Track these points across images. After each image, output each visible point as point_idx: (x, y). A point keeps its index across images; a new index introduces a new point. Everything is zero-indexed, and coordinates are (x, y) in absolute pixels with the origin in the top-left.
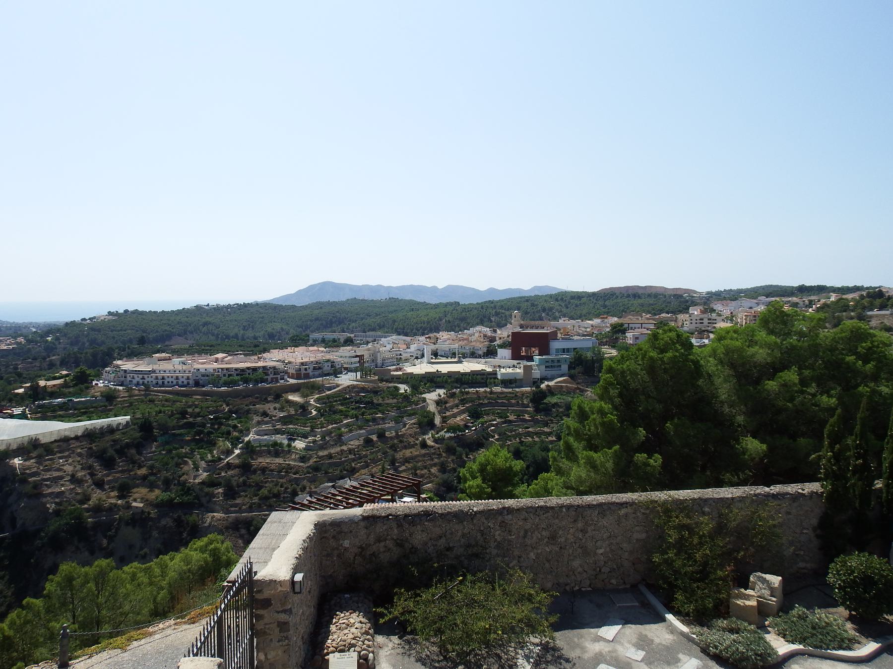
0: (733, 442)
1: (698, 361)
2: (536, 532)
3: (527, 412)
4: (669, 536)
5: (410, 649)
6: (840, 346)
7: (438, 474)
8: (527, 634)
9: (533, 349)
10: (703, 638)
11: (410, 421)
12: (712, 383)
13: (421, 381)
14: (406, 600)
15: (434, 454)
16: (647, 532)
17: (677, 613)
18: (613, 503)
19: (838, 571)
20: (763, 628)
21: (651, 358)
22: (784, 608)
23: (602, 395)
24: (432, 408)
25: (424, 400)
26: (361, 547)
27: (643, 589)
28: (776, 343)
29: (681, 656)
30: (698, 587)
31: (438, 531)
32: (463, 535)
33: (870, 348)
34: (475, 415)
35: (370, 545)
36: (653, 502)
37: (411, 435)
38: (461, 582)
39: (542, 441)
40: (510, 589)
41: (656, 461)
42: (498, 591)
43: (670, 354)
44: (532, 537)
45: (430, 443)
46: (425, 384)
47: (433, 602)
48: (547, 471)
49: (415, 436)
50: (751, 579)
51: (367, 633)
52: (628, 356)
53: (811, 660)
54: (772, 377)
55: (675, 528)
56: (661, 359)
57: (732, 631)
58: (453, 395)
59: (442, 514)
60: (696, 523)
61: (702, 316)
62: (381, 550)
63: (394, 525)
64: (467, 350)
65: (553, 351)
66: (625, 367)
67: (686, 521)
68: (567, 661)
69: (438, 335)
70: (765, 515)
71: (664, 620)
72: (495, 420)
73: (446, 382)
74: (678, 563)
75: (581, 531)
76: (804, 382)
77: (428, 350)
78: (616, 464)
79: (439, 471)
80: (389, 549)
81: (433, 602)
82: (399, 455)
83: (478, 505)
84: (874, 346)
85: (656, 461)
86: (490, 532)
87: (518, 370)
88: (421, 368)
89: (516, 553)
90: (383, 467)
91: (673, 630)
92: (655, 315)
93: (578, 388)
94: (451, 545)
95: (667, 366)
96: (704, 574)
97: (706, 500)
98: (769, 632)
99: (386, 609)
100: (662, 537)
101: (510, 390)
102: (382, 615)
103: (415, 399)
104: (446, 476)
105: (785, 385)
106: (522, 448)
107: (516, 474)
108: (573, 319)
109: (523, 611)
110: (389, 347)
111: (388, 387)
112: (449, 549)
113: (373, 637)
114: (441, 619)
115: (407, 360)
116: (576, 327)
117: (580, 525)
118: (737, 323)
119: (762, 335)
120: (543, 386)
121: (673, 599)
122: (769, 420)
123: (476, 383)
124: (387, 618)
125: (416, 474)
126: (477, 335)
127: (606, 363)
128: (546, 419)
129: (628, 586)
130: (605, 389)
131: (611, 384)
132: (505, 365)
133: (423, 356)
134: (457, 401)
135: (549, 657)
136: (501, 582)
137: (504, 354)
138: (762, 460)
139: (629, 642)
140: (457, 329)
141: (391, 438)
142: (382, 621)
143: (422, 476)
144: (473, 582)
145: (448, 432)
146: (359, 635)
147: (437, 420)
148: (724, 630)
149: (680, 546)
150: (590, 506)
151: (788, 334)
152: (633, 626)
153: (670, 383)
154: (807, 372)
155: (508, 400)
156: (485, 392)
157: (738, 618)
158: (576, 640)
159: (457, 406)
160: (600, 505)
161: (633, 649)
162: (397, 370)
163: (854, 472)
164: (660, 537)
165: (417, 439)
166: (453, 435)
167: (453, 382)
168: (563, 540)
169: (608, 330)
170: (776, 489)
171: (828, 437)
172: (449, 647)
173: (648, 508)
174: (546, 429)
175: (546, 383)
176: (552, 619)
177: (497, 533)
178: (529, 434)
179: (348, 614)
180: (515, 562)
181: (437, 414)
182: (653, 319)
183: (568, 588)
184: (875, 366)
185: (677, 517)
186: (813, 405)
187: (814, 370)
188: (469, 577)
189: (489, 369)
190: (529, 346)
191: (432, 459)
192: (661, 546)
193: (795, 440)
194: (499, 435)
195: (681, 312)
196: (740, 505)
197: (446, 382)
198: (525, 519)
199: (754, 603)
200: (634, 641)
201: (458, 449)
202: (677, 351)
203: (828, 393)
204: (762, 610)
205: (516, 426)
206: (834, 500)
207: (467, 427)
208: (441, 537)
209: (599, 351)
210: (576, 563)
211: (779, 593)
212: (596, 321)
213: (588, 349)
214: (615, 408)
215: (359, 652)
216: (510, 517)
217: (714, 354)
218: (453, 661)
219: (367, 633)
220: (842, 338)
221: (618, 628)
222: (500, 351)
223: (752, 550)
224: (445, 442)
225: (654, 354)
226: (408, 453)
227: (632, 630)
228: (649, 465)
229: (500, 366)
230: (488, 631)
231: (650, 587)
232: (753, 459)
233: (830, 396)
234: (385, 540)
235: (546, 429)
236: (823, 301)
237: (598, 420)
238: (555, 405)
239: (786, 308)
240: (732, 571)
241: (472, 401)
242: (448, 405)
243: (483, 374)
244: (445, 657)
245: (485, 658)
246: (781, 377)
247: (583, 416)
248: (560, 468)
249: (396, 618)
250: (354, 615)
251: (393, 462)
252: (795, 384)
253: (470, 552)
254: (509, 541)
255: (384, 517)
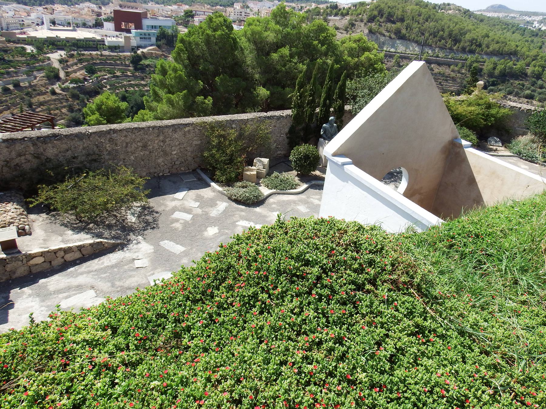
0: (252, 90)
1: (236, 39)
2: (134, 144)
3: (129, 70)
4: (213, 141)
5: (56, 219)
6: (311, 35)
7: (67, 113)
8: (132, 202)
9: (130, 24)
10: (229, 192)
11: (40, 75)
12: (243, 53)
13: (44, 44)
14: (47, 192)
15: (63, 99)
16: (201, 140)
17: (217, 181)
18: (181, 124)
19: (294, 154)
20: (258, 184)
21: (208, 34)
22: (269, 174)
23: (176, 58)
24: (56, 65)
25: (49, 59)
26: (5, 161)
27: (199, 171)
28: (279, 30)
29: (218, 202)
30: (228, 168)
31: (64, 146)
32: (84, 148)
33: (326, 37)
34: (91, 71)
35: (13, 159)
36: (204, 122)
37: (42, 85)
38: (85, 177)
39: (141, 90)
40: (119, 178)
41: (209, 101)
42: (111, 180)
43: (219, 33)
44: (131, 147)
45: (58, 91)
46: (48, 46)
47: (67, 190)
48: (144, 109)
49: (44, 86)
50: (255, 161)
51: (21, 214)
52: (194, 32)
53: (279, 196)
54: (275, 51)
55: (216, 137)
56: (214, 36)
57: (243, 187)
58: (72, 56)
59: (66, 135)
60: (228, 134)
61: (241, 10)
62: (469, 343)
63: (30, 144)
64: (80, 22)
65: (144, 26)
66: (191, 39)
67: (223, 133)
68: (157, 212)
69: (53, 7)
70: (263, 128)
71: (210, 186)
72: (106, 75)
73: (65, 45)
74: (218, 156)
75: (162, 141)
76: (292, 56)
77: (47, 18)
78: (185, 103)
79: (68, 111)
80: (29, 161)
81: (67, 190)
82: (35, 100)
83: (92, 129)
84: (327, 36)
85: (209, 101)
86: (103, 145)
87: (120, 40)
88: (43, 33)
89: (122, 157)
90: (21, 108)
91: (214, 190)
92: (213, 6)
93: (164, 55)
94: (76, 155)
95: (217, 41)
96: (231, 161)
97: (234, 121)
98: (261, 186)
99: (34, 198)
100: (209, 143)
101: (116, 54)
102: (31, 203)
103: (41, 57)
104: (74, 114)
105: (282, 57)
106: (127, 95)
107: (123, 111)
108: (158, 4)
109: (129, 189)
110: (11, 13)
111: (16, 48)
112: (74, 158)
113: (27, 216)
114: (74, 199)
115: (29, 26)
116: (161, 11)
117: (161, 138)
118: (261, 17)
119: (272, 25)
120: (139, 52)
121: (214, 175)
122: (277, 79)
123: (89, 47)
124: (35, 204)
125: (51, 114)
126: (86, 9)
127: (179, 36)
128: (142, 75)
129: (191, 171)
130: (179, 54)
131: (182, 50)
132: (109, 35)
133: (43, 23)
134: (75, 61)
135: (146, 212)
136: (113, 175)
137: (109, 26)
138: (267, 100)
139: (191, 199)
140: (69, 3)
141: (26, 87)
142: (31, 206)
143: (56, 115)
144: (94, 176)
145: (71, 83)
146: (16, 216)
147: (62, 75)
148: (240, 187)
149: (219, 146)
150: (167, 127)
151: (286, 26)
152: (193, 191)
153: (219, 52)
154: (294, 49)
155: (115, 61)
156: (97, 54)
157: (247, 181)
158: (161, 201)
159: (76, 64)
160: (173, 125)
161: (193, 202)
162: (21, 33)
163: (308, 104)
164: (208, 142)
165: (48, 88)
166: (75, 85)
167: (71, 46)
168: (151, 147)
169: (182, 14)
170: (270, 114)
171: (298, 85)
172: (83, 215)
173: (201, 127)
174: (143, 82)
175: (141, 50)
176: (147, 192)
177: (108, 145)
178: (131, 85)
179: (4, 204)
180: (121, 163)
181: (61, 70)
182: (212, 9)
183: (156, 175)
184: (326, 48)
185: (217, 131)
186: (295, 69)
187: (298, 48)
188: (91, 173)
189: (99, 38)
190: (127, 21)
191: (62, 103)
192: (208, 147)
193: (284, 89)
194: (110, 86)
195: (229, 6)
196: (251, 123)
197: (65, 45)
198: (126, 136)
199: (255, 173)
200: (194, 198)
201: (81, 96)
202: (223, 31)
203: (302, 62)
204: (259, 176)
205: (122, 80)
206: (297, 118)
207: (85, 80)
208: (68, 150)
209: (176, 29)
210: (160, 161)
211: (267, 167)
212: (174, 7)
213: (169, 27)
214: (185, 67)
215: (18, 226)
216: (115, 135)
217: (245, 35)
218: (86, 222)
219: (21, 214)
220: (313, 30)
221: (185, 193)
222: (105, 24)
223: (256, 146)
224: (70, 90)
225: (209, 32)
226: (41, 98)
227: (193, 193)
228: (205, 103)
229: (106, 36)
230: (106, 203)
231: (202, 170)
232: (262, 100)
233: (303, 64)
234: (25, 155)
235: (143, 82)
236: (308, 7)
237: (173, 75)
238: (148, 66)
239: (287, 9)
240: (245, 158)
241: (88, 61)
242: (69, 63)
243: (94, 41)
244: (80, 221)
245: (107, 218)
246: (280, 52)
247: (164, 72)
248: (151, 107)
249: (42, 203)
250: (10, 205)
251: (30, 105)
252: (287, 56)
253: (90, 159)
254: (116, 150)
255: (21, 139)
